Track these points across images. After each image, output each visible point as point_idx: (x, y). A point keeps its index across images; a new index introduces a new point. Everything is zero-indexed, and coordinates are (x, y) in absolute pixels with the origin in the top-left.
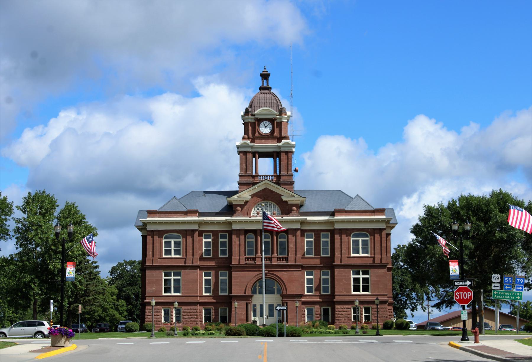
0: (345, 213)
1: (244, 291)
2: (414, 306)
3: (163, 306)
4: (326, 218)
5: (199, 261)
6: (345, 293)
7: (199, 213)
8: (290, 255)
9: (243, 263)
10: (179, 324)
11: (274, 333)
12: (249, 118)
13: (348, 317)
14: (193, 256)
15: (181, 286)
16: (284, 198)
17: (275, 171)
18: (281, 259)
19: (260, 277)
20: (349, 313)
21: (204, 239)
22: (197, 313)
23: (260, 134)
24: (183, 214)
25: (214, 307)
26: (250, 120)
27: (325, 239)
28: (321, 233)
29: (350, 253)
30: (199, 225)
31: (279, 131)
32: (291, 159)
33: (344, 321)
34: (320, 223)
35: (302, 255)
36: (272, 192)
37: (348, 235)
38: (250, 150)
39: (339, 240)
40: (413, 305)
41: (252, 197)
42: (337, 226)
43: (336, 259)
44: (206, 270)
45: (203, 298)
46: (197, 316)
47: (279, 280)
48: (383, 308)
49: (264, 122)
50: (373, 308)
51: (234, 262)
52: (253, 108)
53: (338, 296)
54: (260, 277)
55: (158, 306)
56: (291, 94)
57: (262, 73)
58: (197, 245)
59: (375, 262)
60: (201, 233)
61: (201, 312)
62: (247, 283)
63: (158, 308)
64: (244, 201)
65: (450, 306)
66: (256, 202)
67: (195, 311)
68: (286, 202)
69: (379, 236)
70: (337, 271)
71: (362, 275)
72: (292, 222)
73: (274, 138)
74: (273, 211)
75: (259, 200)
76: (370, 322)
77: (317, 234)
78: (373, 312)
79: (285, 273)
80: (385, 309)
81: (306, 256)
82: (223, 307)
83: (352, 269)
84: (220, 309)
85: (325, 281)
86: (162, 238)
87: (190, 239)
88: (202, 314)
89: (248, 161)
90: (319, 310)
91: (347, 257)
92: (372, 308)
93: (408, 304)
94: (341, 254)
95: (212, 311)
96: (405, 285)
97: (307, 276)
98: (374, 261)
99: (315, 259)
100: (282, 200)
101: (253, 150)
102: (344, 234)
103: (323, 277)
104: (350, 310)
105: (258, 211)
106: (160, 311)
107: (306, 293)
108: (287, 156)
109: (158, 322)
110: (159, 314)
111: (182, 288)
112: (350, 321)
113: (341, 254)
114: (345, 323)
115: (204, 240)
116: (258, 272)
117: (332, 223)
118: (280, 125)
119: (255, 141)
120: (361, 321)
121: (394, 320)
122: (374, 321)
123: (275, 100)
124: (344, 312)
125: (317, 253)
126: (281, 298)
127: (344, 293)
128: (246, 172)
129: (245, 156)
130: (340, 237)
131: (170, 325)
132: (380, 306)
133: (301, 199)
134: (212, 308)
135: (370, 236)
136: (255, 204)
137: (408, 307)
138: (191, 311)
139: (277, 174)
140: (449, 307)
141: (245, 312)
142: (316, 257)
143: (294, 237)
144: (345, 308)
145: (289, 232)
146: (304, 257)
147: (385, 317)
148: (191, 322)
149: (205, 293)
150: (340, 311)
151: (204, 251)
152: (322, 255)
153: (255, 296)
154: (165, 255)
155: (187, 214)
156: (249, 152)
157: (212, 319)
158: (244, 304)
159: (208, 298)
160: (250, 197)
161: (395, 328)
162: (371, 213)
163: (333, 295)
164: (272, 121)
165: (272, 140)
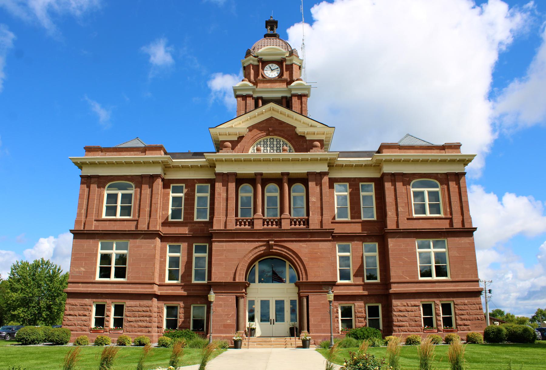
1: (232, 276)
3: (94, 300)
5: (162, 226)
6: (408, 279)
8: (313, 214)
9: (232, 226)
10: (119, 332)
12: (251, 59)
13: (416, 321)
14: (150, 216)
15: (127, 266)
19: (260, 251)
20: (417, 313)
21: (172, 193)
22: (150, 313)
24: (138, 152)
25: (183, 303)
26: (251, 62)
29: (410, 212)
31: (289, 75)
32: (306, 104)
35: (332, 217)
36: (281, 123)
37: (406, 183)
38: (251, 93)
41: (250, 131)
42: (388, 169)
43: (389, 222)
44: (172, 242)
45: (165, 288)
46: (150, 318)
47: (294, 256)
48: (474, 304)
49: (270, 65)
50: (457, 305)
51: (218, 225)
53: (396, 285)
54: (260, 251)
55: (86, 299)
58: (158, 199)
60: (166, 184)
61: (160, 312)
62: (236, 263)
63: (86, 303)
66: (256, 137)
67: (148, 309)
69: (456, 185)
70: (392, 243)
72: (314, 161)
73: (283, 81)
74: (283, 146)
75: (261, 134)
79: (303, 245)
80: (477, 306)
81: (337, 219)
82: (198, 304)
86: (104, 187)
87: (146, 190)
88: (163, 315)
89: (247, 107)
90: (363, 309)
91: (408, 219)
92: (454, 304)
94: (397, 215)
95: (181, 312)
98: (451, 224)
99: (352, 224)
101: (255, 96)
104: (417, 307)
106: (88, 307)
109: (84, 327)
110: (87, 313)
111: (129, 269)
112: (419, 328)
113: (397, 215)
114: (411, 332)
115: (172, 195)
116: (257, 243)
118: (290, 68)
120: (439, 327)
122: (461, 327)
123: (283, 43)
124: (408, 311)
125: (356, 212)
126: (296, 290)
127: (407, 279)
129: (244, 102)
131: (104, 332)
133: (327, 130)
135: (441, 184)
136: (254, 141)
138: (141, 309)
141: (234, 312)
144: (409, 305)
145: (310, 178)
146: (334, 221)
147: (478, 319)
148: (140, 329)
150: (400, 311)
151: (170, 212)
152: (363, 219)
153: (252, 285)
155: (145, 152)
157: (179, 324)
158: (231, 299)
159: (172, 287)
163: (386, 282)
164: (280, 63)
165: (279, 84)
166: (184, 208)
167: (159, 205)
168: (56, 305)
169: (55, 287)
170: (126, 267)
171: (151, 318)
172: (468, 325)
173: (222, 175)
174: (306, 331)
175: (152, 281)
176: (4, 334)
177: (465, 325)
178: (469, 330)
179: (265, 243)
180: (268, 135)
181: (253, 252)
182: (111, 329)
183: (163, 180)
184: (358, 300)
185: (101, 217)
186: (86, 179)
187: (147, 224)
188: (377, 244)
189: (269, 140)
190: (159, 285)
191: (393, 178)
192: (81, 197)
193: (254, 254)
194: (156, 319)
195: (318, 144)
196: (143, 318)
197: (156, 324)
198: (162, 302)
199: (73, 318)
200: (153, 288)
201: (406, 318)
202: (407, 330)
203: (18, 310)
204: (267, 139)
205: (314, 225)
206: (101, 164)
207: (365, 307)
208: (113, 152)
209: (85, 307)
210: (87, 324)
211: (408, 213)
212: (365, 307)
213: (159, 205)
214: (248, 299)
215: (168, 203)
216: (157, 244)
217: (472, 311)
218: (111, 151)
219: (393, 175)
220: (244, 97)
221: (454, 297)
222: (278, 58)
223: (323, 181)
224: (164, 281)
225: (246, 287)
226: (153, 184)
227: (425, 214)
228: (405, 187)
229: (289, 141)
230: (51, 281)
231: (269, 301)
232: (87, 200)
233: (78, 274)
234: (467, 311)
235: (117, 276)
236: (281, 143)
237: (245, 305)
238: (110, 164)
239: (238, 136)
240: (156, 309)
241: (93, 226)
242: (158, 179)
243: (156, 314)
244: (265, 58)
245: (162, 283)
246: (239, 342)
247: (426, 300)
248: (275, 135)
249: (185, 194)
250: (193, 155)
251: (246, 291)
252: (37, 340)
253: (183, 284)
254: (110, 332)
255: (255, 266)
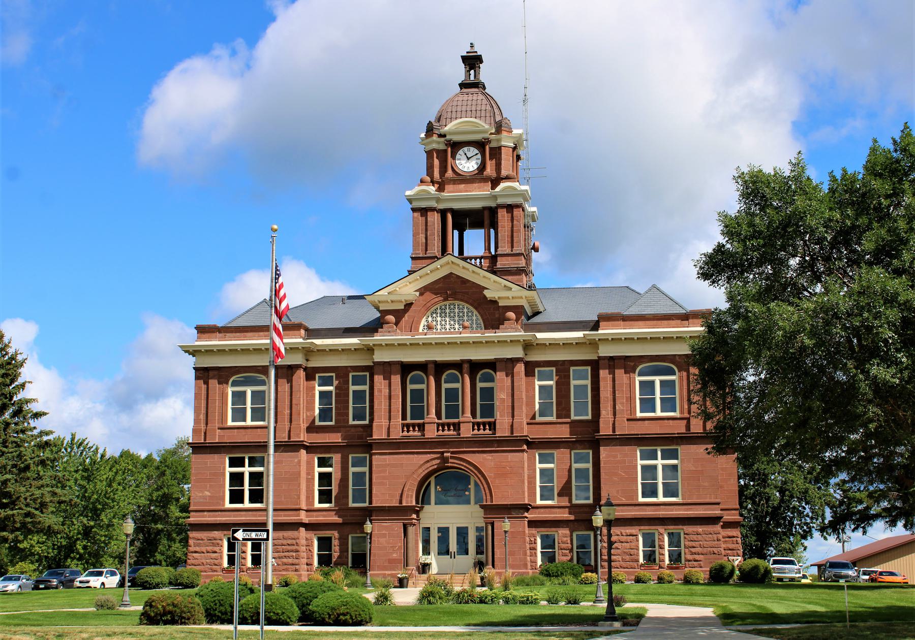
0: (622, 323)
1: (398, 498)
2: (807, 530)
4: (579, 334)
5: (307, 432)
6: (624, 501)
7: (307, 329)
9: (397, 434)
11: (278, 614)
13: (631, 555)
14: (291, 421)
16: (488, 294)
17: (488, 248)
18: (480, 426)
20: (633, 544)
22: (297, 547)
23: (457, 172)
25: (338, 533)
27: (579, 381)
28: (572, 369)
30: (306, 355)
31: (496, 166)
33: (622, 563)
34: (567, 345)
36: (464, 281)
37: (630, 370)
38: (433, 204)
39: (610, 383)
40: (805, 527)
41: (421, 294)
42: (605, 351)
43: (602, 425)
45: (315, 514)
46: (297, 553)
47: (476, 472)
49: (465, 149)
50: (687, 534)
51: (378, 434)
52: (443, 122)
56: (525, 96)
57: (465, 54)
58: (301, 398)
59: (691, 430)
60: (310, 374)
61: (309, 545)
62: (404, 480)
63: (214, 536)
64: (401, 302)
65: (864, 528)
66: (429, 304)
67: (294, 542)
68: (494, 302)
70: (604, 452)
71: (662, 459)
72: (502, 343)
73: (485, 180)
75: (437, 300)
76: (681, 565)
77: (563, 369)
78: (687, 543)
80: (715, 536)
81: (538, 419)
82: (357, 533)
83: (639, 445)
84: (352, 537)
85: (581, 473)
86: (227, 383)
88: (313, 549)
89: (429, 228)
90: (569, 539)
92: (685, 534)
93: (796, 525)
94: (615, 414)
95: (335, 543)
96: (788, 490)
97: (540, 463)
98: (688, 427)
100: (485, 296)
101: (442, 206)
102: (620, 368)
103: (575, 466)
104: (634, 537)
105: (443, 323)
106: (218, 541)
107: (539, 502)
108: (510, 215)
110: (217, 549)
112: (635, 564)
113: (615, 414)
114: (624, 568)
115: (318, 389)
116: (429, 455)
117: (593, 344)
118: (496, 153)
119: (446, 187)
120: (661, 563)
121: (737, 561)
123: (488, 105)
124: (622, 542)
125: (563, 410)
127: (622, 500)
128: (426, 250)
129: (424, 218)
130: (611, 376)
132: (705, 529)
134: (335, 534)
135: (679, 371)
136: (427, 309)
137: (795, 532)
138: (285, 542)
139: (490, 252)
140: (861, 530)
141: (401, 544)
142: (426, 383)
143: (509, 378)
144: (624, 534)
146: (533, 421)
147: (714, 554)
148: (285, 567)
149: (320, 502)
151: (317, 412)
152: (573, 417)
153: (426, 507)
154: (233, 420)
156: (433, 209)
157: (334, 560)
158: (398, 526)
159: (324, 513)
160: (417, 294)
161: (740, 578)
162: (679, 321)
164: (480, 145)
166: (335, 406)
167: (302, 405)
168: (101, 527)
169: (97, 492)
170: (263, 489)
171: (299, 553)
172: (700, 561)
173: (383, 364)
174: (491, 567)
175: (297, 507)
176: (55, 583)
177: (695, 561)
178: (701, 567)
179: (438, 455)
180: (446, 299)
181: (424, 468)
182: (249, 568)
183: (306, 369)
184: (562, 527)
185: (227, 423)
186: (202, 372)
187: (287, 432)
188: (591, 452)
189: (448, 307)
190: (307, 511)
191: (611, 363)
192: (197, 396)
193: (426, 469)
194: (305, 554)
195: (511, 315)
196: (288, 553)
197: (305, 561)
198: (311, 532)
199: (201, 556)
200: (299, 516)
201: (618, 550)
202: (618, 567)
203: (29, 541)
204: (446, 305)
205: (503, 431)
206: (221, 351)
207: (571, 536)
208: (236, 332)
209: (214, 541)
210: (219, 563)
211: (629, 412)
212: (571, 536)
213: (302, 405)
214: (422, 526)
215: (314, 401)
216: (302, 459)
217: (707, 543)
218: (232, 332)
219: (612, 358)
220: (424, 211)
221: (684, 524)
222: (478, 137)
223: (515, 370)
224: (313, 505)
225: (417, 513)
226: (292, 376)
227: (655, 412)
228: (628, 375)
229: (476, 308)
230: (88, 479)
231: (448, 528)
232: (205, 401)
233: (202, 500)
234: (701, 542)
235: (252, 500)
236: (465, 310)
237: (416, 535)
238: (233, 351)
239: (404, 303)
240: (304, 542)
241: (216, 437)
242: (298, 371)
243: (305, 548)
244: (456, 138)
245: (310, 508)
246: (405, 580)
247: (647, 527)
248: (456, 299)
249: (336, 388)
250: (343, 332)
251: (418, 516)
252: (162, 584)
253: (337, 508)
254: (248, 572)
255: (430, 482)
